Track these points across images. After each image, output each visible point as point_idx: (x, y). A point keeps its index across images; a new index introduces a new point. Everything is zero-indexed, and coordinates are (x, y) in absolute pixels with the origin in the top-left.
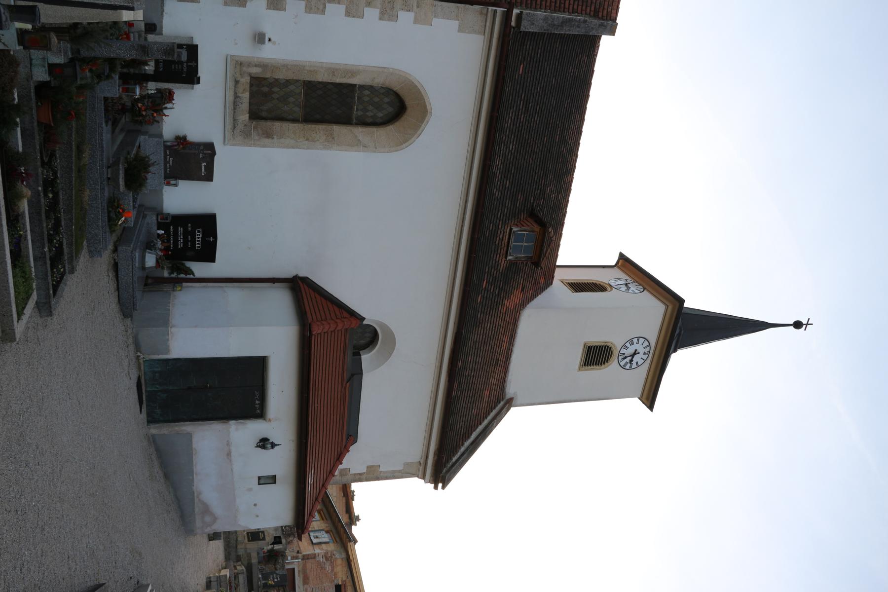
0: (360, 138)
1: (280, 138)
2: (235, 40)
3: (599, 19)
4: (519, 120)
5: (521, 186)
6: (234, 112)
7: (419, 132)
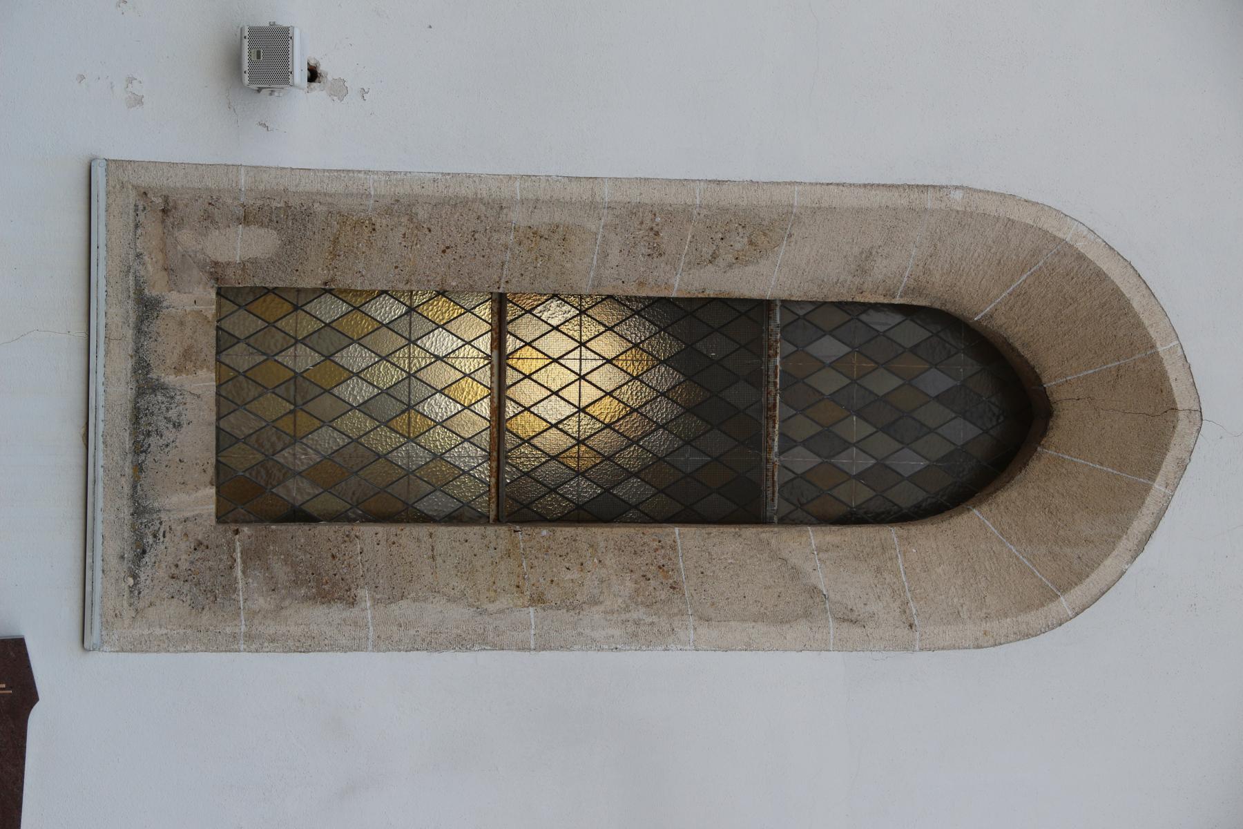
0: (821, 580)
1: (392, 600)
2: (131, 80)
6: (139, 468)
7: (1139, 526)
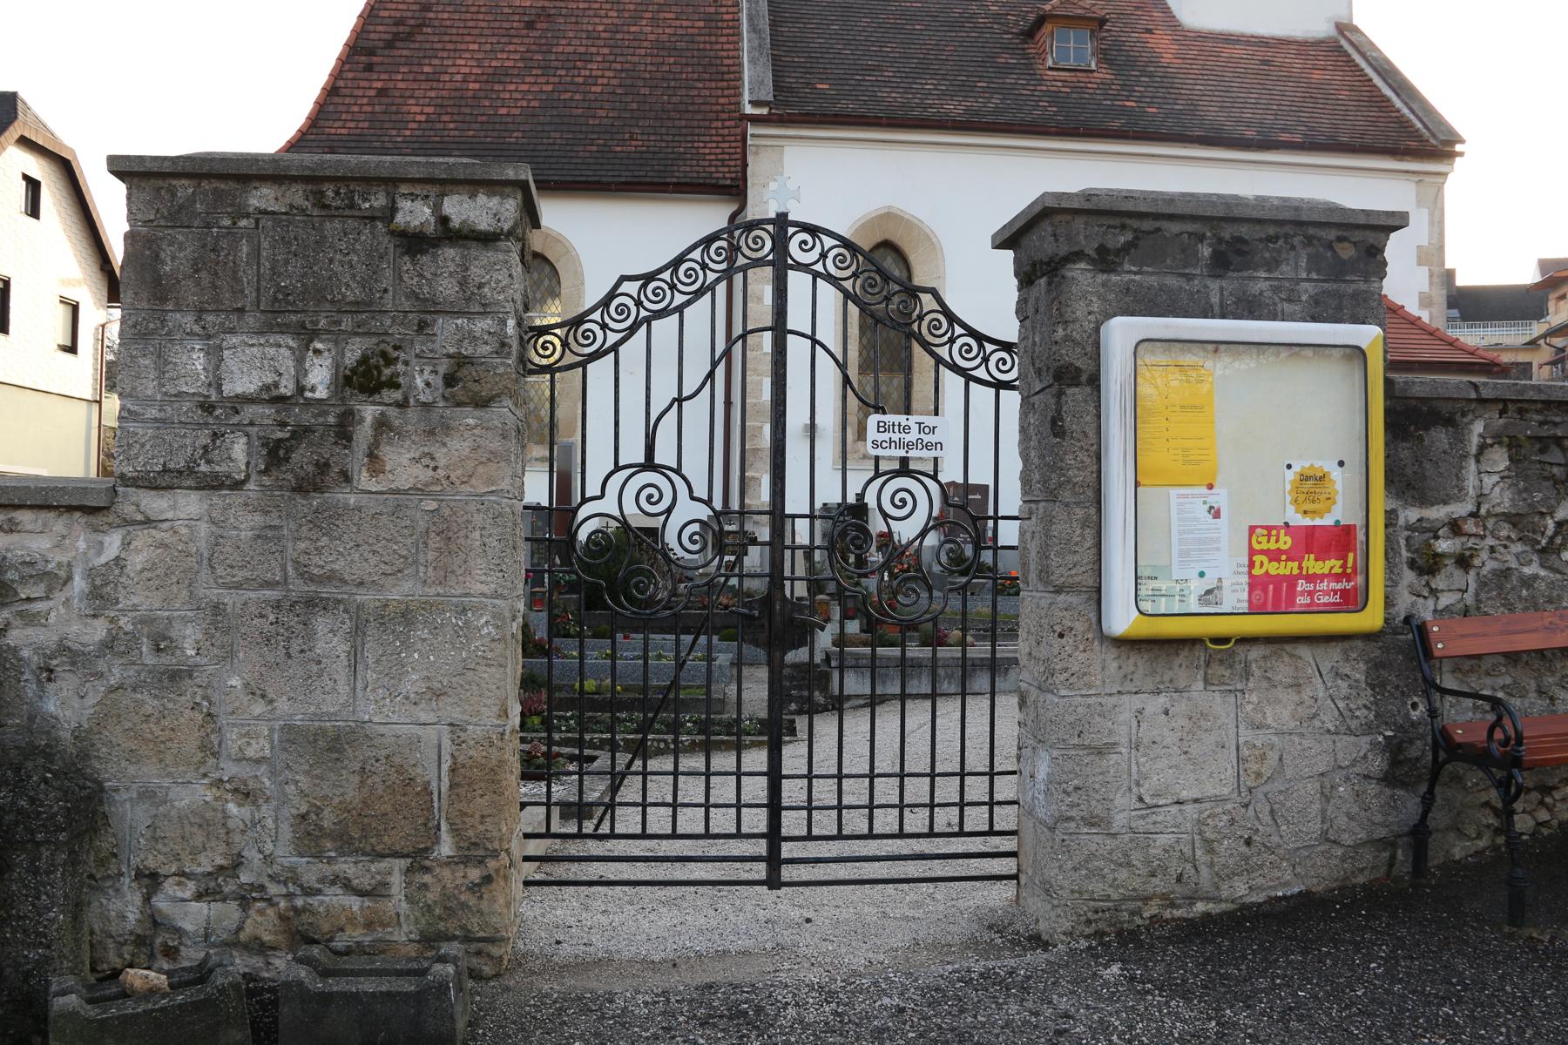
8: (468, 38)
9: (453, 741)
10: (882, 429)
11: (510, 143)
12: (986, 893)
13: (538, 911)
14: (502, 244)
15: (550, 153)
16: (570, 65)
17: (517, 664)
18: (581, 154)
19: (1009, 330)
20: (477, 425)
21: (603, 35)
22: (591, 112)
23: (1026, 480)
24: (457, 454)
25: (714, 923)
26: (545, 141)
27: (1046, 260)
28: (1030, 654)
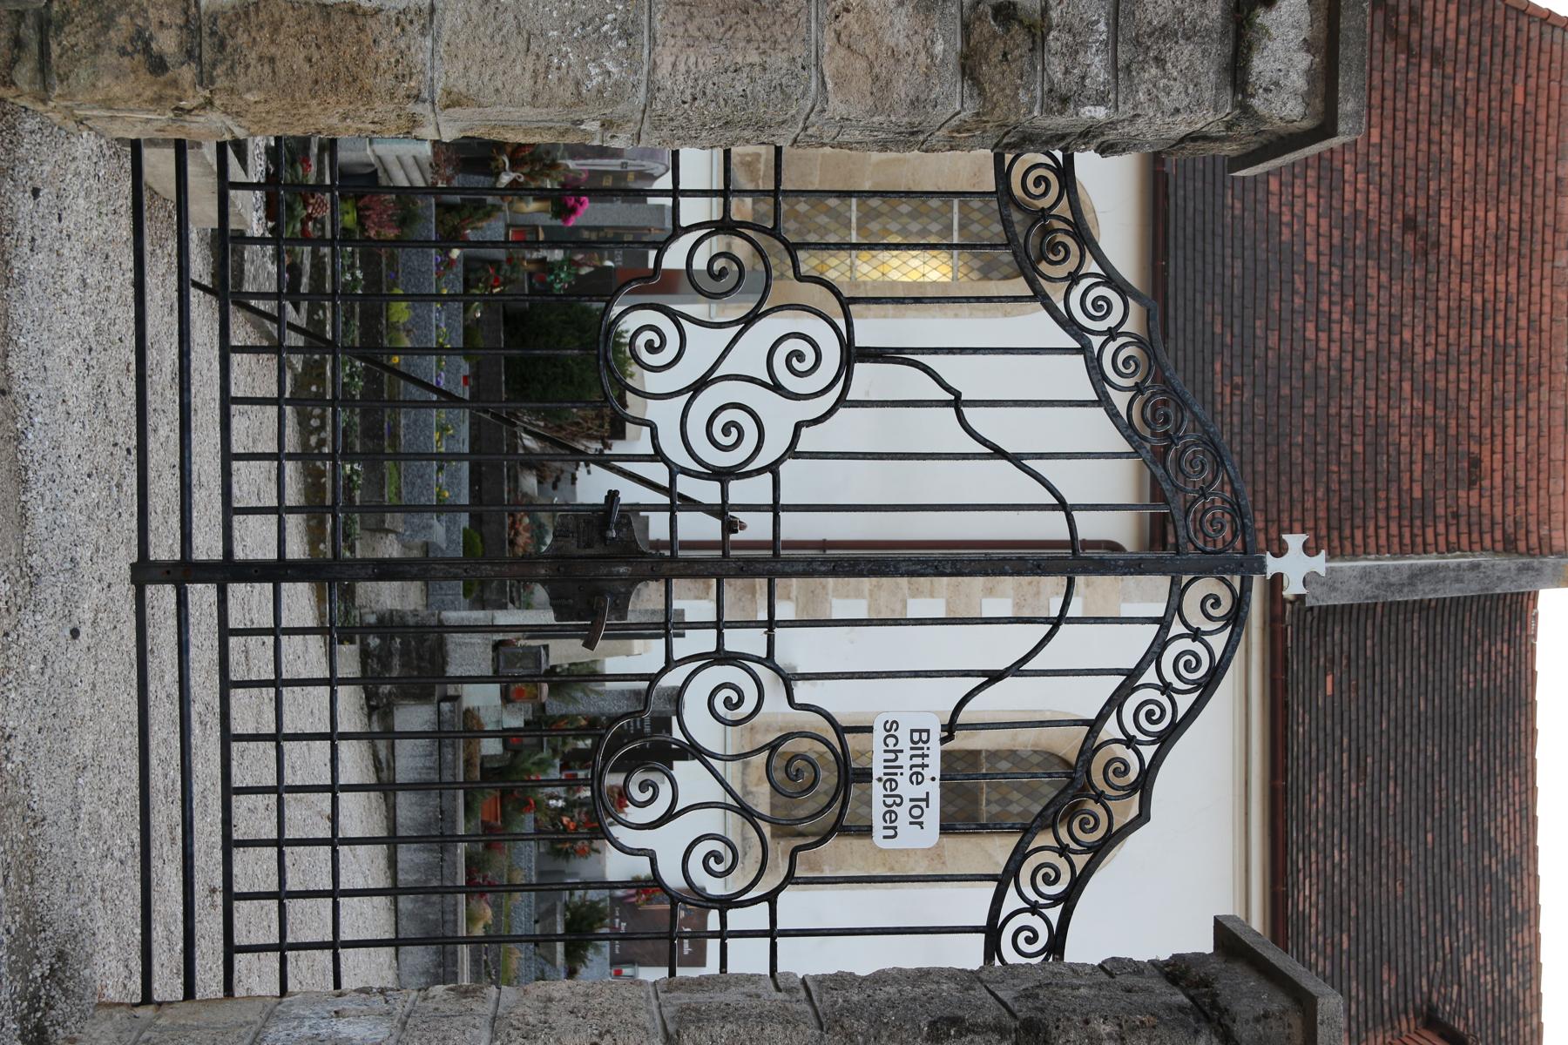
3: (1521, 555)
4: (1345, 796)
5: (1385, 948)
8: (1388, 126)
9: (404, 12)
10: (916, 736)
11: (1224, 196)
12: (113, 949)
13: (84, 166)
14: (1227, 96)
15: (1209, 259)
16: (1348, 289)
17: (526, 132)
18: (1209, 309)
19: (1083, 948)
20: (932, 57)
21: (1396, 340)
22: (1274, 324)
23: (842, 981)
24: (886, 24)
25: (70, 468)
26: (1228, 251)
27: (1222, 1002)
28: (550, 1000)
